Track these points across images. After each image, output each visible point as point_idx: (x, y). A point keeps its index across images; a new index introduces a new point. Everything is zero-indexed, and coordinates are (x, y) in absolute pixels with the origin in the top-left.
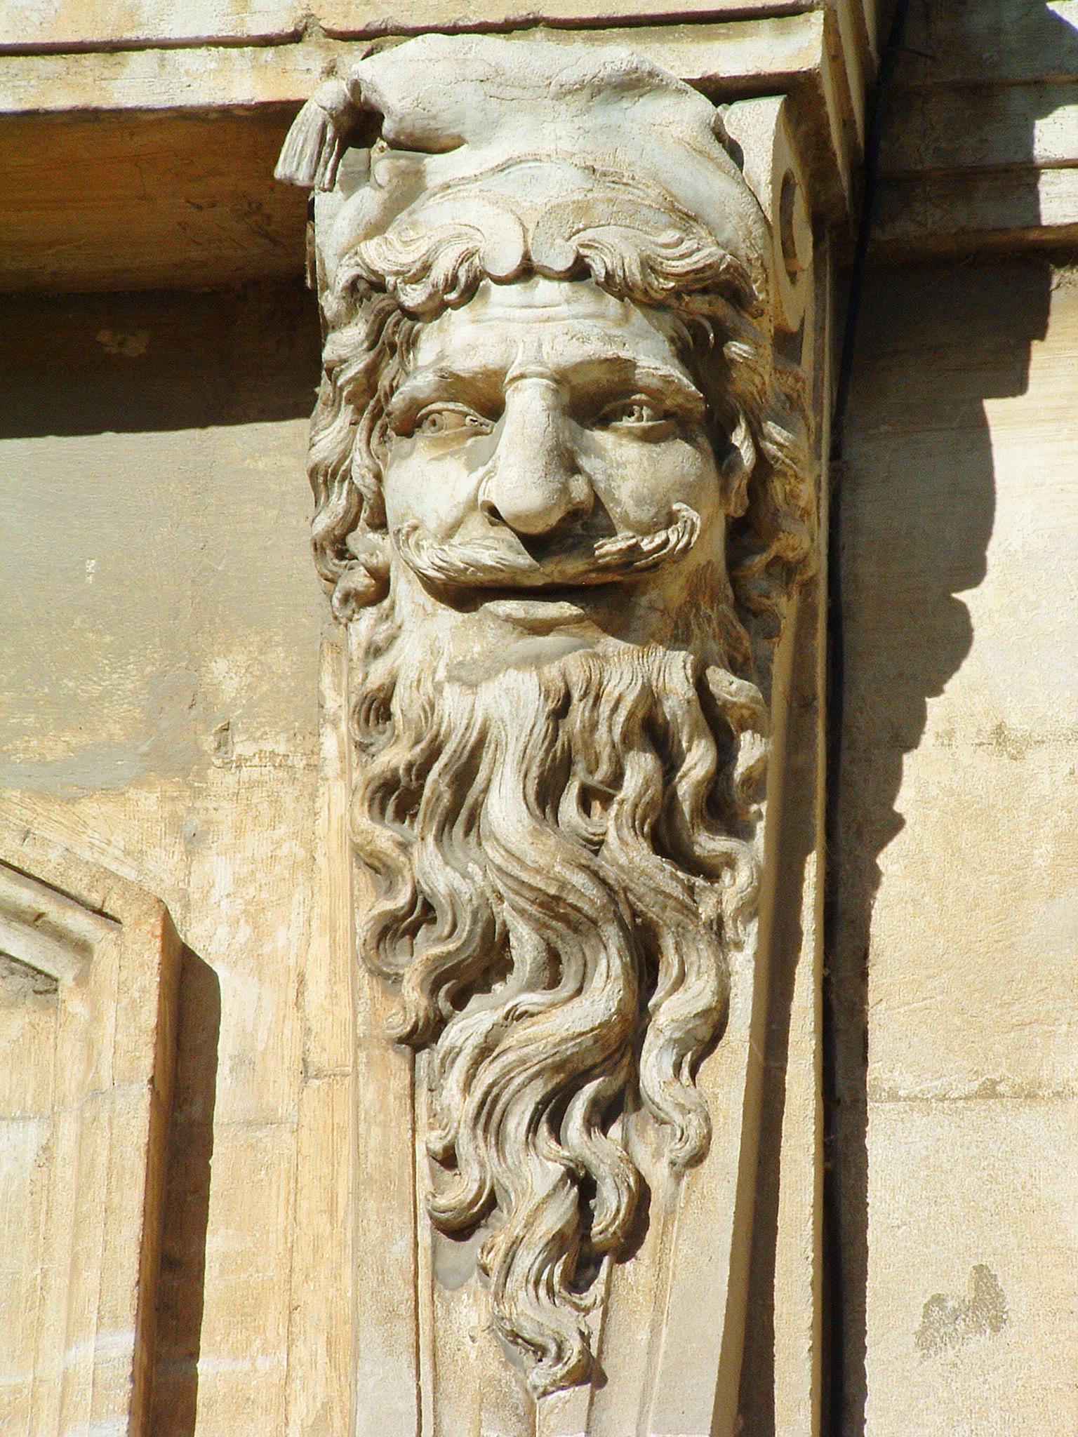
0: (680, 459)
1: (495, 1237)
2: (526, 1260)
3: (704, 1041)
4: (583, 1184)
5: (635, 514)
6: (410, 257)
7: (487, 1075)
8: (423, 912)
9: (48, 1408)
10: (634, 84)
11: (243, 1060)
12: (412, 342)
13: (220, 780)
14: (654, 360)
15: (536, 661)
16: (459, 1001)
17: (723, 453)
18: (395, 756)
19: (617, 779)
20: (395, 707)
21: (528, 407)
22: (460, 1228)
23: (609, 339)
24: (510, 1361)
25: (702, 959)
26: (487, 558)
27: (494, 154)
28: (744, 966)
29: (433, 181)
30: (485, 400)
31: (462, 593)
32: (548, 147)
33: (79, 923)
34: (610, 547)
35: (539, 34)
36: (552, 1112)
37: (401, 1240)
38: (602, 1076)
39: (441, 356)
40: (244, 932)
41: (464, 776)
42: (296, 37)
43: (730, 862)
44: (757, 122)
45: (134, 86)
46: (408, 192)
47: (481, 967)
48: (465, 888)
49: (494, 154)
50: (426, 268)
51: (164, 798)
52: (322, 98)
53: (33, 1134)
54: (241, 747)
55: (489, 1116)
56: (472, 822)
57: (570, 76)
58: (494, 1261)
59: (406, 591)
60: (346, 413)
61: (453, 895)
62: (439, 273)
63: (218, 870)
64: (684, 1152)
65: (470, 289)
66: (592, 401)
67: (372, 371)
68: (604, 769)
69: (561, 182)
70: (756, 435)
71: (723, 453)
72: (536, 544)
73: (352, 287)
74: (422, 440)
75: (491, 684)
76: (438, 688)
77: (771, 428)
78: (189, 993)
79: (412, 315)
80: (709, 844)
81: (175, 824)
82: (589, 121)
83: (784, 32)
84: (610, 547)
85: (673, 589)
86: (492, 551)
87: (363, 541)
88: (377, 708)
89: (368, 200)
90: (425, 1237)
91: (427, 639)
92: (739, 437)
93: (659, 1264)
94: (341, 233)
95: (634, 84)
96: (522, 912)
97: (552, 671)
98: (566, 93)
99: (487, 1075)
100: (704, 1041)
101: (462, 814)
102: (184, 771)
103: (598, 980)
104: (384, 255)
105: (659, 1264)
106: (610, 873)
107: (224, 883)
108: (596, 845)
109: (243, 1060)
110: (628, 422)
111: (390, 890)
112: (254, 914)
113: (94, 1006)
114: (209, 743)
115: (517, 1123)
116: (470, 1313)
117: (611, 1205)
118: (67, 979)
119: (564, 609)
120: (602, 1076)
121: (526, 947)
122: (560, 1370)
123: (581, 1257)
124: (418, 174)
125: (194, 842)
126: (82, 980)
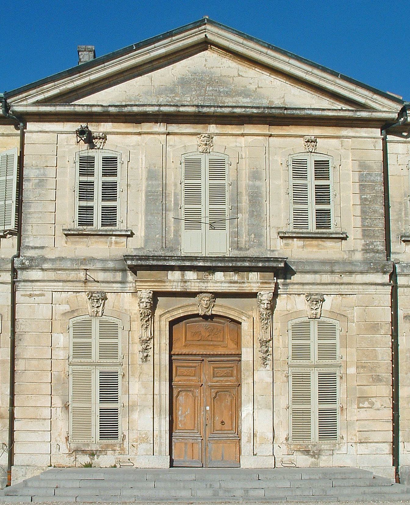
101: (263, 315)
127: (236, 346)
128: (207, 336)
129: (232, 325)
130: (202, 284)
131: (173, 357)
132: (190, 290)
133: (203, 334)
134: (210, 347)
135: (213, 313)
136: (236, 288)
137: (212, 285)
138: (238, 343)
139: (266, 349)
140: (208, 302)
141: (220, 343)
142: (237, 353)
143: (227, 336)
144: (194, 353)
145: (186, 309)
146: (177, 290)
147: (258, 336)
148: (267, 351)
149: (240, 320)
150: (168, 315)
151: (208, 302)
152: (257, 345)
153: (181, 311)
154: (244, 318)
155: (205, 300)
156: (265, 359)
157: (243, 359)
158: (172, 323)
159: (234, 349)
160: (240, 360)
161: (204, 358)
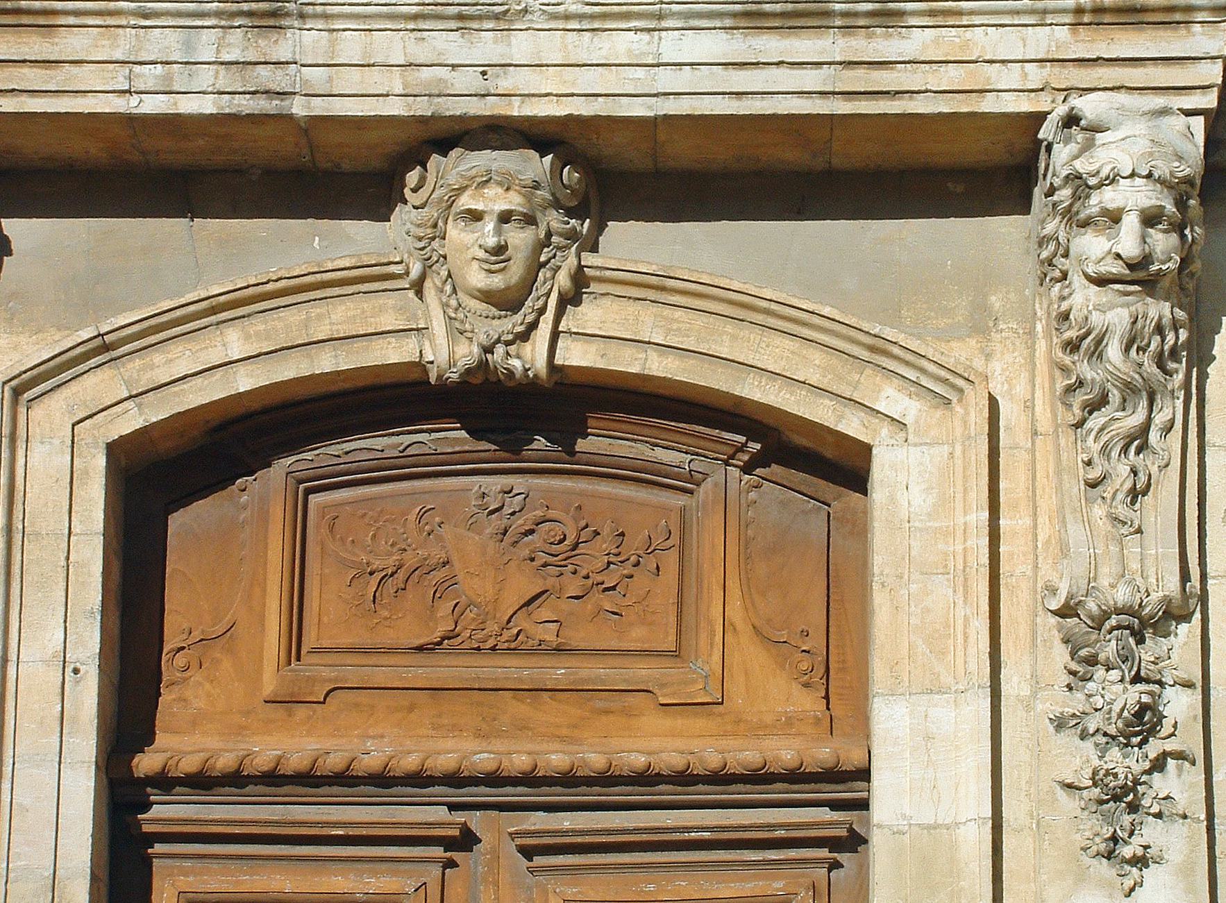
0: (1174, 238)
1: (1107, 490)
2: (1120, 496)
3: (1168, 428)
4: (1135, 472)
5: (1161, 257)
6: (1093, 168)
7: (1104, 439)
8: (1081, 383)
9: (959, 533)
10: (1165, 112)
11: (1007, 428)
12: (1088, 196)
13: (996, 336)
14: (1170, 208)
15: (1128, 305)
16: (1090, 413)
17: (1183, 236)
18: (1072, 334)
19: (1149, 345)
20: (1071, 317)
21: (1131, 222)
22: (1093, 485)
23: (1158, 199)
24: (1114, 526)
25: (1168, 402)
26: (1114, 271)
27: (1120, 134)
28: (1179, 403)
29: (1097, 143)
30: (1114, 217)
31: (1101, 281)
32: (1137, 133)
33: (960, 382)
34: (1154, 268)
35: (1123, 91)
36: (1125, 449)
37: (1076, 489)
38: (1139, 439)
39: (1101, 202)
40: (1006, 386)
41: (1099, 341)
42: (1042, 90)
43: (1177, 371)
44: (1198, 123)
45: (988, 105)
46: (1088, 146)
47: (1100, 402)
48: (1098, 378)
49: (1120, 134)
50: (1098, 172)
51: (978, 342)
52: (1061, 110)
53: (946, 449)
54: (1002, 326)
55: (1105, 451)
56: (1100, 356)
57: (1146, 109)
58: (1108, 495)
59: (1077, 280)
60: (1058, 219)
61: (1093, 380)
62: (1103, 174)
63: (996, 367)
64: (1163, 463)
65: (1112, 180)
66: (1150, 219)
67: (1071, 205)
68: (1146, 341)
69: (1143, 145)
70: (1192, 230)
71: (1183, 236)
72: (1131, 267)
73: (1067, 177)
74: (1089, 230)
75: (1115, 314)
76: (1090, 312)
77: (1196, 228)
78: (993, 403)
79: (1090, 188)
80: (1172, 365)
81: (982, 350)
82: (1150, 124)
83: (1204, 94)
84: (1154, 268)
85: (1165, 283)
86: (1117, 268)
87: (1059, 261)
88: (1065, 316)
89: (1073, 148)
90: (1082, 487)
91: (1083, 297)
92: (1187, 232)
93: (1155, 497)
94: (1063, 158)
95: (1165, 112)
96: (1116, 386)
97: (1133, 309)
98: (1145, 114)
99: (1104, 439)
100: (1168, 428)
101: (1097, 352)
102: (984, 333)
103: (1140, 409)
104: (1081, 166)
105: (1155, 497)
106: (1145, 375)
107: (999, 371)
108: (1140, 365)
109: (1007, 428)
110: (1160, 226)
111: (1069, 377)
112: (1009, 381)
113: (966, 409)
114: (991, 324)
115: (1115, 454)
116: (1099, 511)
117: (1142, 478)
118: (955, 400)
119: (1137, 288)
120: (1139, 439)
121: (1115, 396)
122: (1132, 530)
123: (1135, 494)
124: (1094, 139)
125: (988, 357)
126: (960, 401)
127: (810, 703)
128: (511, 601)
129: (775, 499)
130: (446, 44)
131: (163, 812)
132: (320, 107)
133: (476, 586)
134: (551, 712)
135: (574, 355)
136: (811, 80)
137: (553, 46)
138: (835, 667)
139: (1135, 695)
140: (519, 239)
141: (642, 671)
142: (822, 754)
143: (723, 605)
144: (371, 761)
145: (289, 323)
146: (189, 106)
147: (1047, 572)
148: (1144, 722)
149: (852, 426)
150: (99, 385)
151: (519, 239)
152: (1035, 660)
153: (233, 341)
154: (892, 399)
155: (479, 209)
156: (1123, 796)
157: (881, 811)
158: (159, 479)
159: (788, 724)
160: (855, 842)
161: (475, 820)
